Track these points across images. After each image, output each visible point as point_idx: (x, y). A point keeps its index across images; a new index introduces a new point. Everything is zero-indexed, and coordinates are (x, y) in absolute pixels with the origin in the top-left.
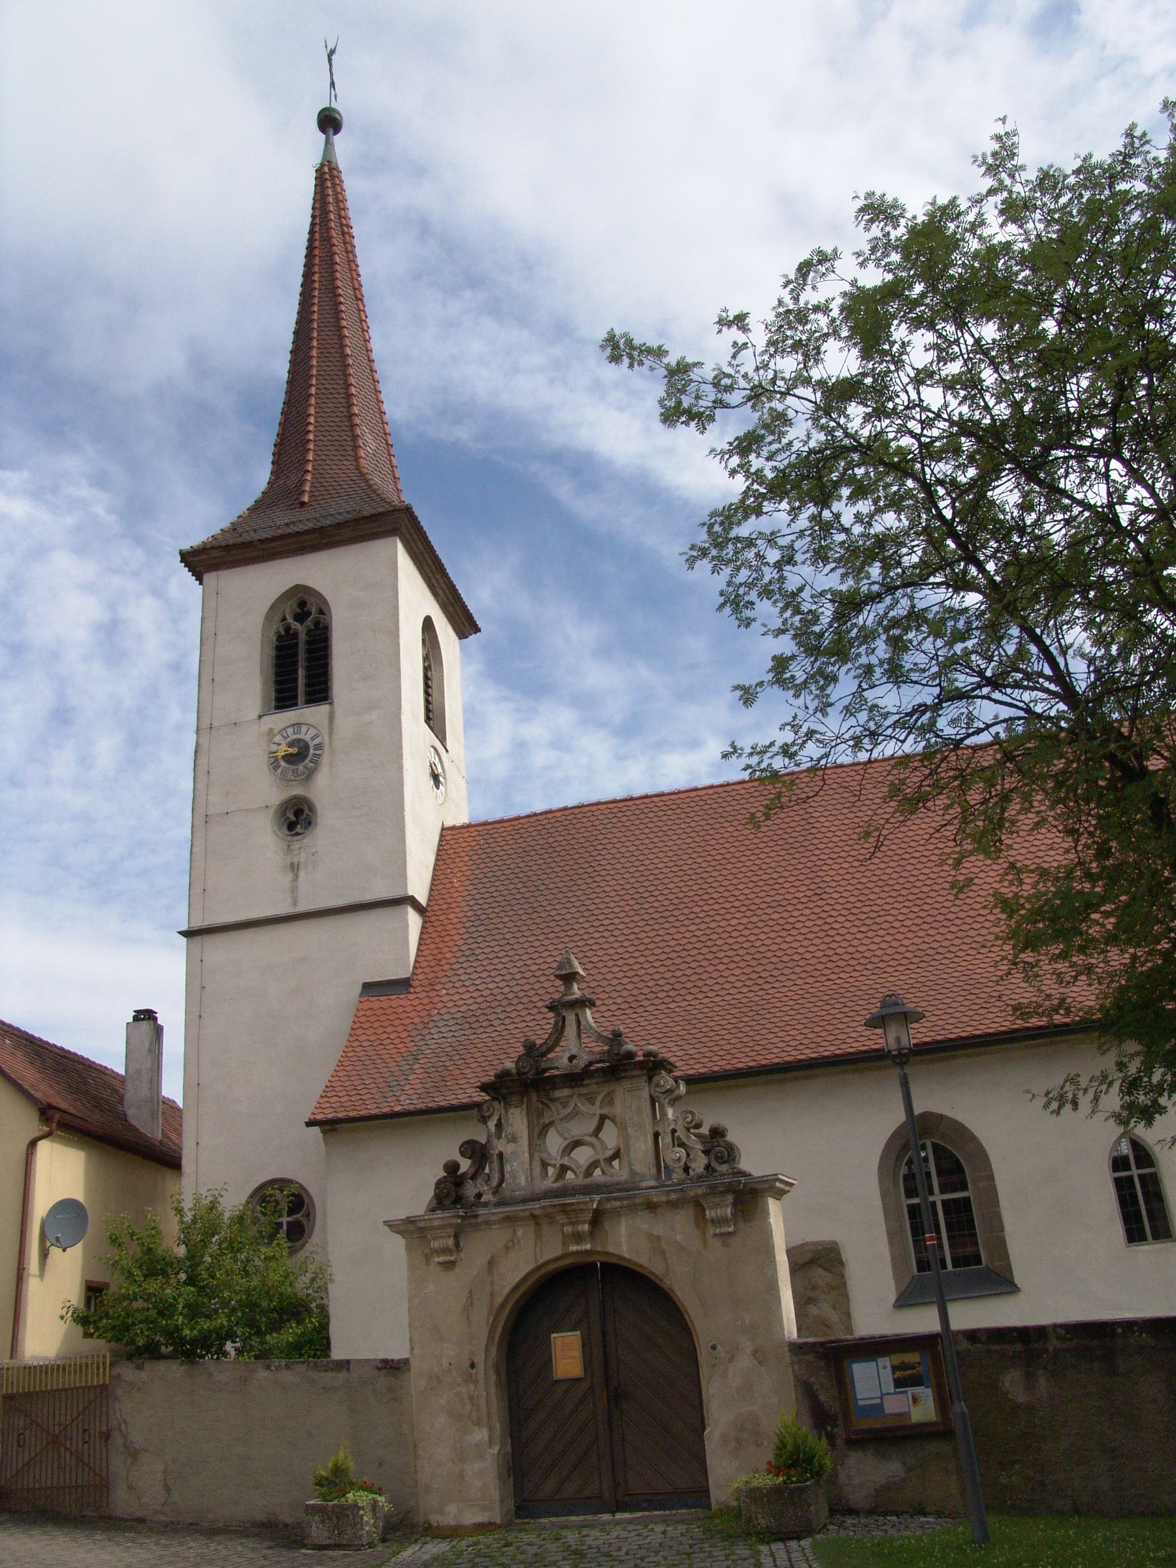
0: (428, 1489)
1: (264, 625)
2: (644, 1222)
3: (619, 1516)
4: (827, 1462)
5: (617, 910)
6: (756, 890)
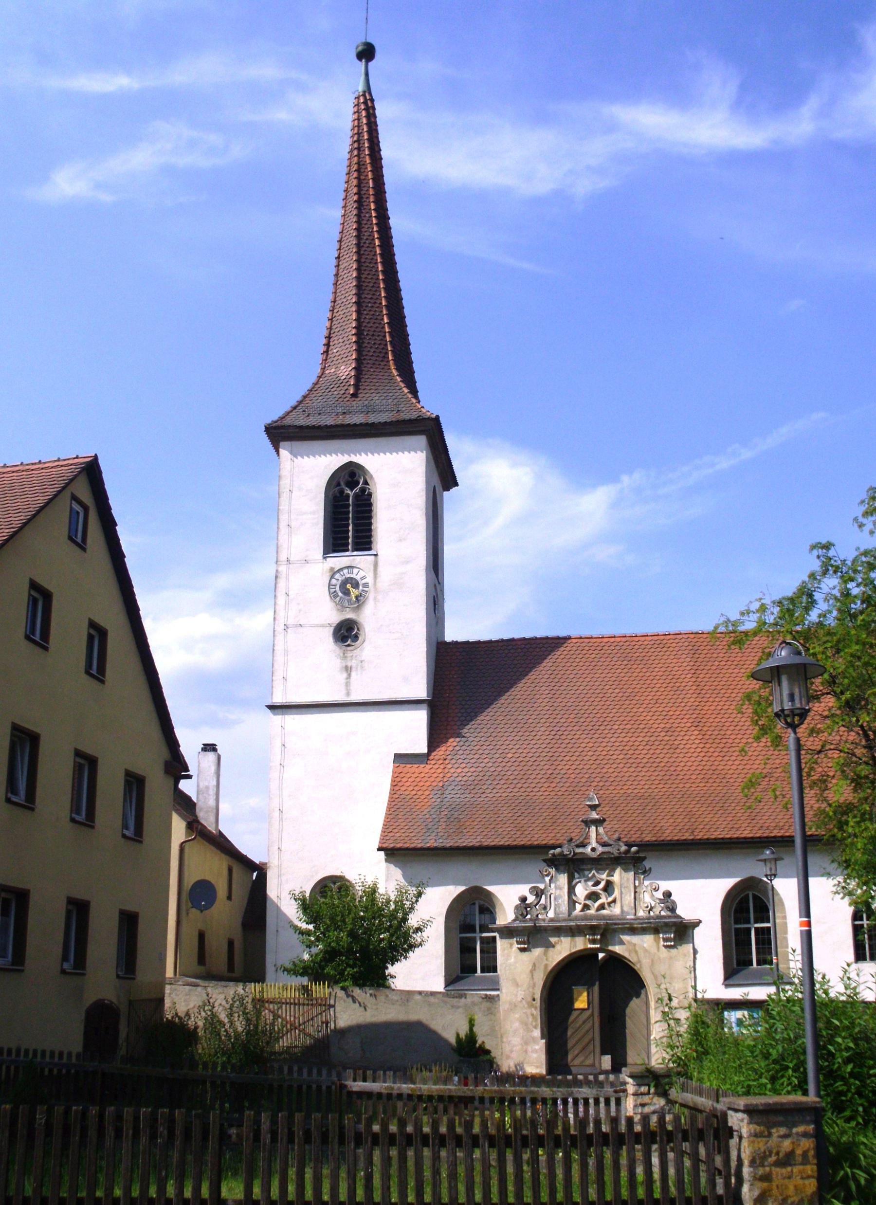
0: (508, 1057)
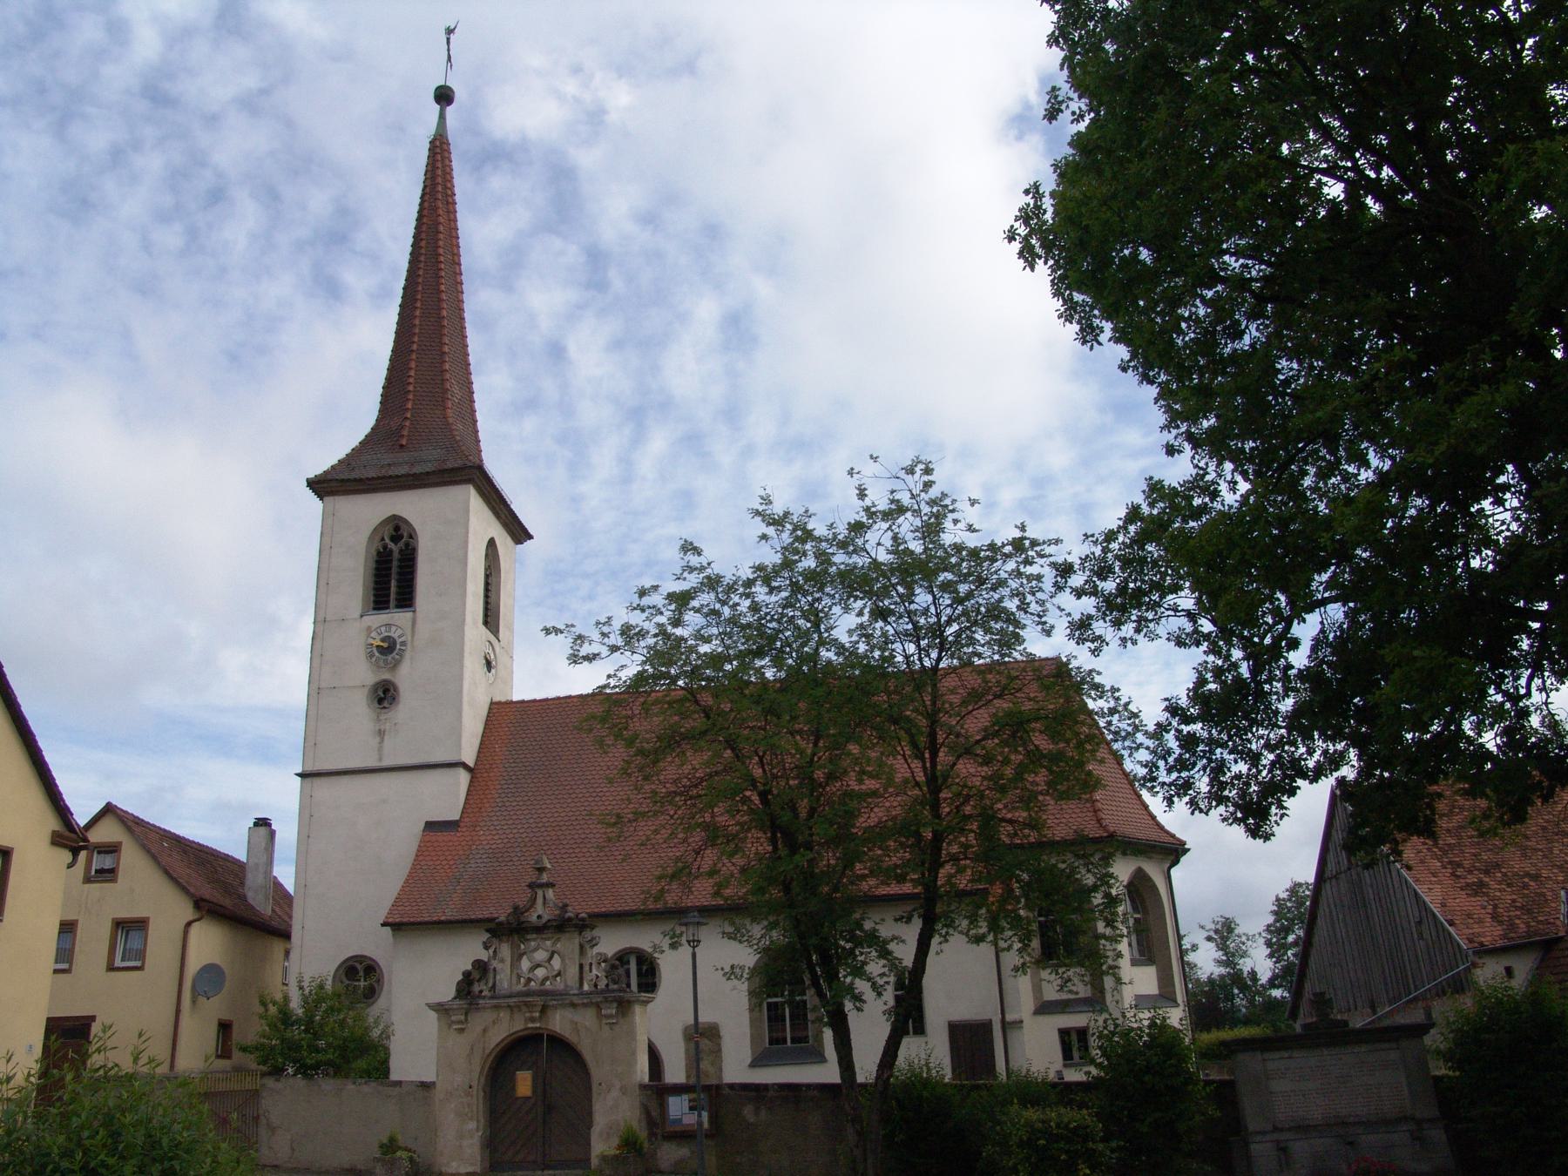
1: (368, 542)
2: (569, 1014)
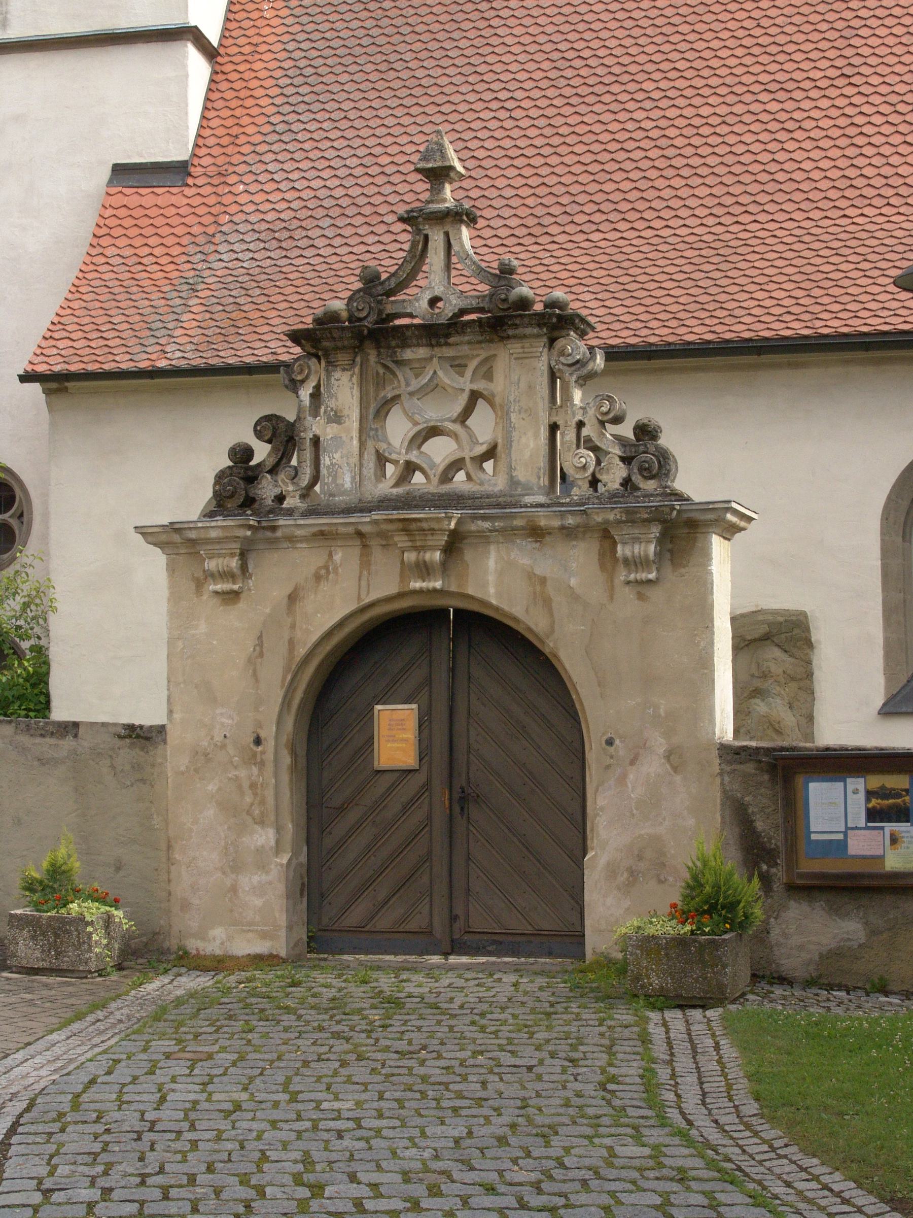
0: (185, 906)
3: (453, 959)
4: (758, 911)
5: (522, 76)
6: (748, 60)
